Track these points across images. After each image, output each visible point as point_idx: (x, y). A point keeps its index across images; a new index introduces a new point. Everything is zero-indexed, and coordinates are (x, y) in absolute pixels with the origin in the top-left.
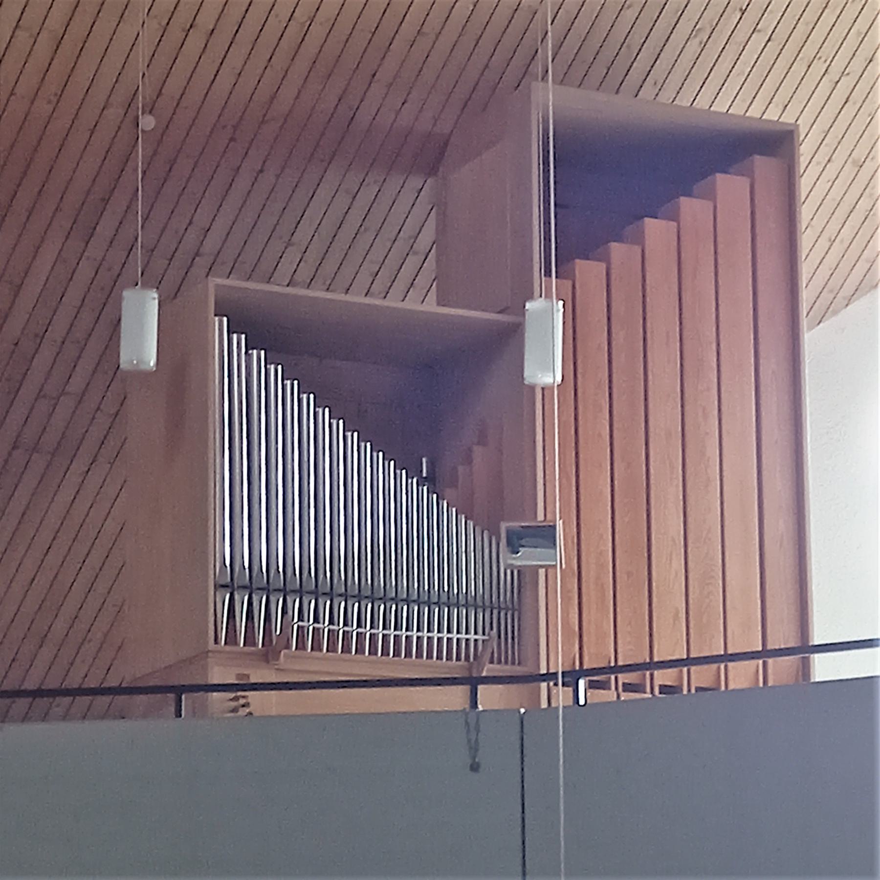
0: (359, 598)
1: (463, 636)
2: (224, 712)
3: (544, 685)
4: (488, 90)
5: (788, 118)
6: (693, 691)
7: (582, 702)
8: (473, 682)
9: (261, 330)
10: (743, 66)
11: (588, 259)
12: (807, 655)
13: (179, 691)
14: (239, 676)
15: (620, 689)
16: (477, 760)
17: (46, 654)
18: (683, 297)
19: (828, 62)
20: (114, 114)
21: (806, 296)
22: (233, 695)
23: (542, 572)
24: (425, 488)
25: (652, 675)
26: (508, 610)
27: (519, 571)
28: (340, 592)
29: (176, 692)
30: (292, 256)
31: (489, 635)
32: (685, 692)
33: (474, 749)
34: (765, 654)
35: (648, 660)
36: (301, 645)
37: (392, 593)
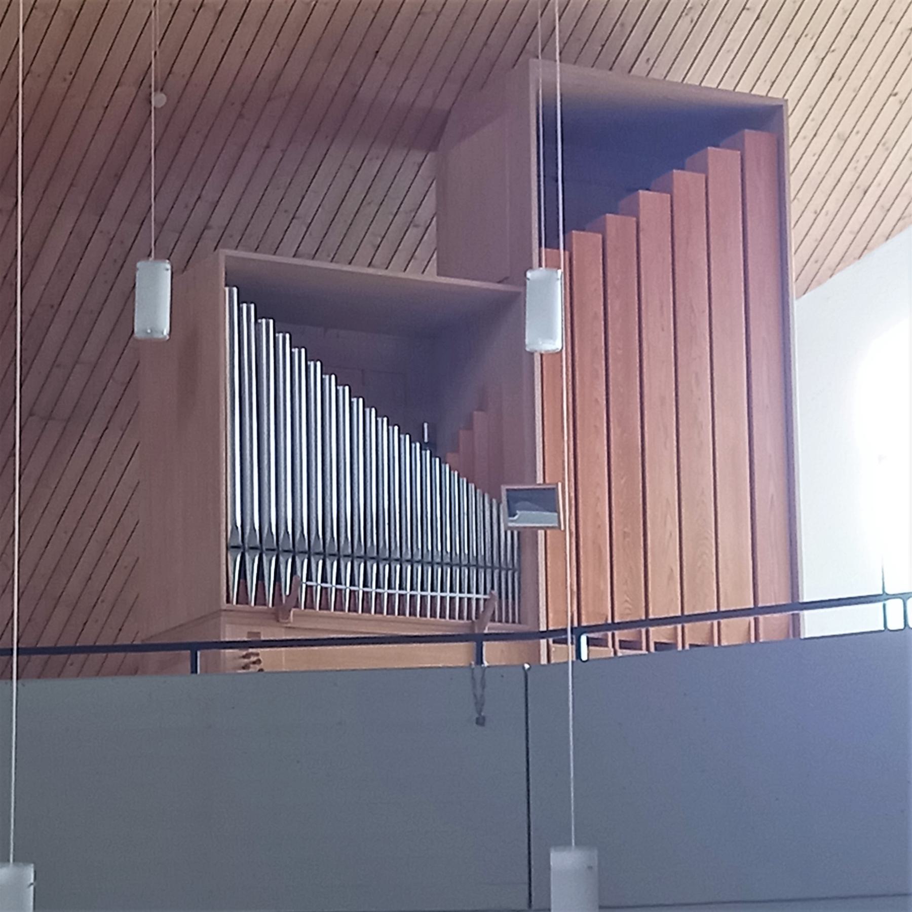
0: (365, 558)
1: (481, 596)
2: (236, 668)
3: (543, 642)
4: (486, 67)
5: (776, 93)
6: (687, 647)
7: (584, 657)
8: (478, 639)
9: (271, 301)
10: (732, 44)
11: (584, 230)
12: (796, 612)
13: (193, 648)
14: (250, 634)
15: (617, 644)
16: (483, 714)
17: (61, 614)
18: (677, 268)
19: (814, 39)
20: (126, 92)
21: (794, 263)
22: (244, 653)
23: (541, 533)
24: (428, 452)
25: (647, 632)
26: (510, 569)
27: (519, 534)
28: (346, 553)
29: (194, 649)
30: (297, 229)
31: (491, 594)
32: (680, 648)
33: (479, 704)
34: (756, 611)
35: (643, 618)
36: (310, 605)
37: (395, 554)
